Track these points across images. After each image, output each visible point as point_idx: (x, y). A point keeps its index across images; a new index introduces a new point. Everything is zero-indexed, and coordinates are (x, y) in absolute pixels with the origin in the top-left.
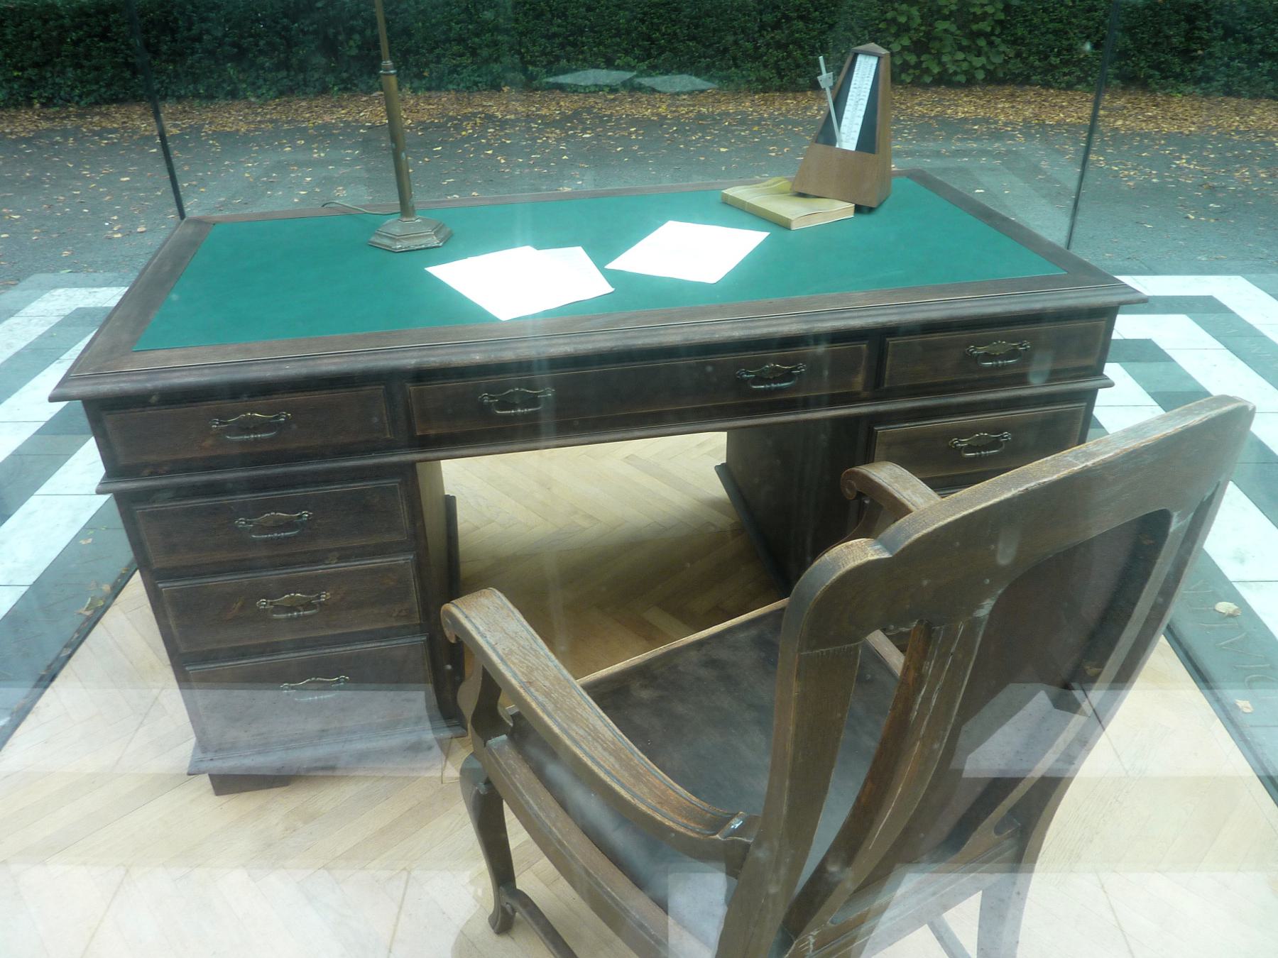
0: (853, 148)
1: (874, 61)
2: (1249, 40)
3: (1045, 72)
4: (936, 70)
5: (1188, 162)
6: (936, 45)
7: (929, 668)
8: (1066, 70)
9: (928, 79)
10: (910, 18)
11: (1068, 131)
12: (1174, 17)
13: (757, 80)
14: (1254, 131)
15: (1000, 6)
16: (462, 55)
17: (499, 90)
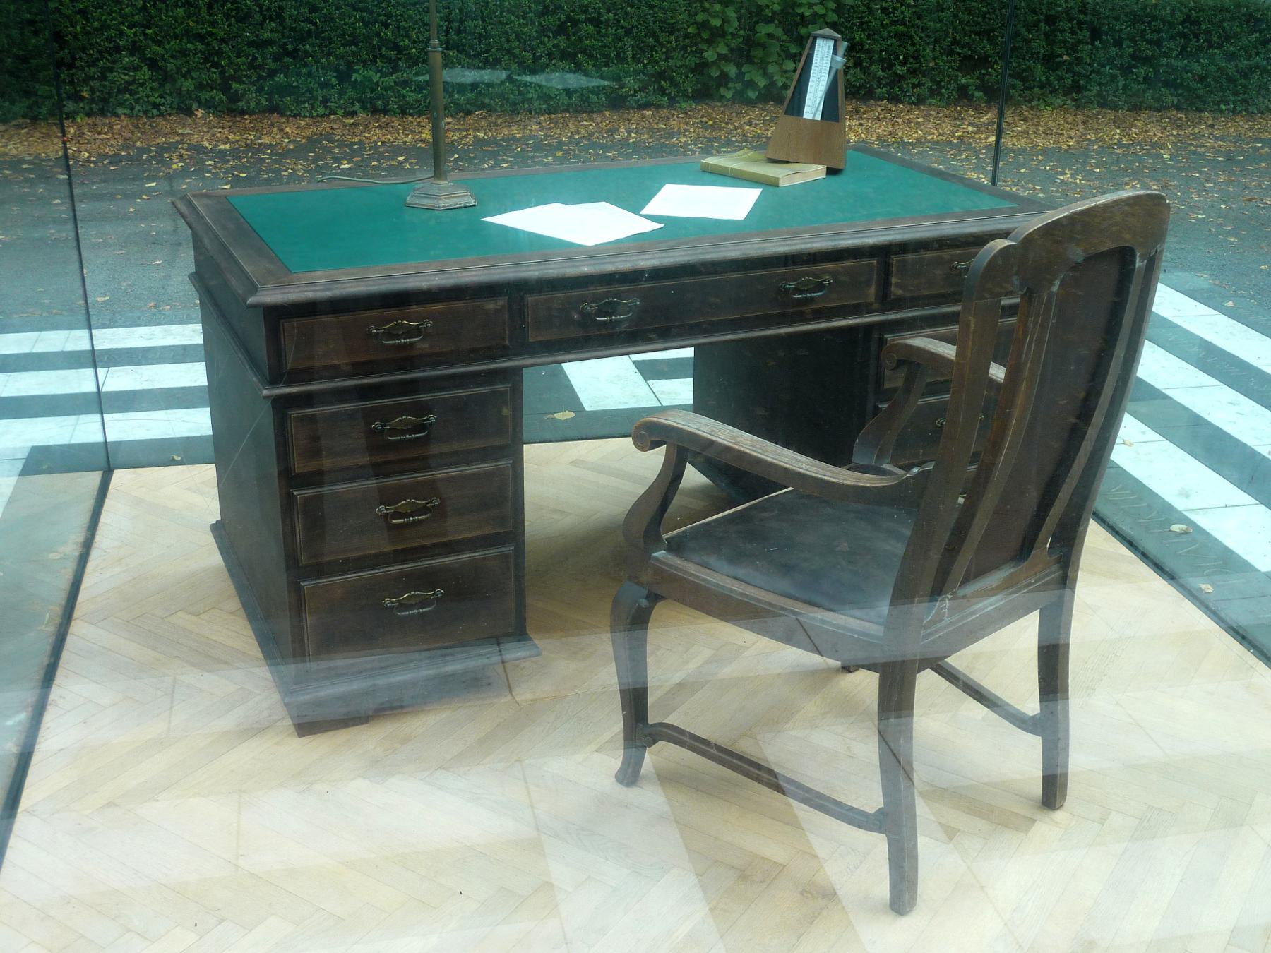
0: (818, 118)
1: (831, 43)
2: (1118, 43)
3: (891, 84)
4: (762, 83)
5: (1072, 176)
6: (758, 53)
7: (1031, 322)
8: (915, 81)
9: (752, 94)
10: (725, 21)
11: (932, 149)
12: (1032, 18)
13: (539, 98)
14: (1139, 144)
15: (832, 5)
16: (136, 69)
17: (189, 112)
